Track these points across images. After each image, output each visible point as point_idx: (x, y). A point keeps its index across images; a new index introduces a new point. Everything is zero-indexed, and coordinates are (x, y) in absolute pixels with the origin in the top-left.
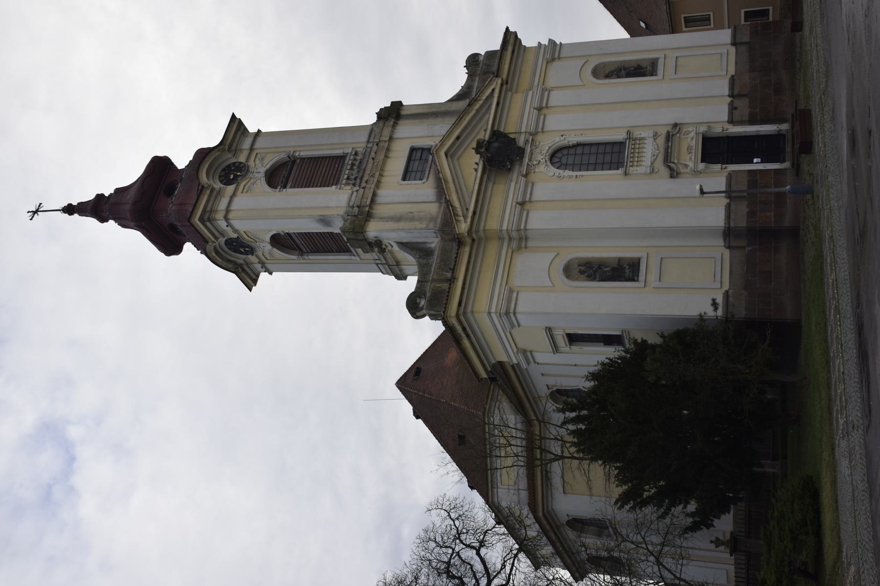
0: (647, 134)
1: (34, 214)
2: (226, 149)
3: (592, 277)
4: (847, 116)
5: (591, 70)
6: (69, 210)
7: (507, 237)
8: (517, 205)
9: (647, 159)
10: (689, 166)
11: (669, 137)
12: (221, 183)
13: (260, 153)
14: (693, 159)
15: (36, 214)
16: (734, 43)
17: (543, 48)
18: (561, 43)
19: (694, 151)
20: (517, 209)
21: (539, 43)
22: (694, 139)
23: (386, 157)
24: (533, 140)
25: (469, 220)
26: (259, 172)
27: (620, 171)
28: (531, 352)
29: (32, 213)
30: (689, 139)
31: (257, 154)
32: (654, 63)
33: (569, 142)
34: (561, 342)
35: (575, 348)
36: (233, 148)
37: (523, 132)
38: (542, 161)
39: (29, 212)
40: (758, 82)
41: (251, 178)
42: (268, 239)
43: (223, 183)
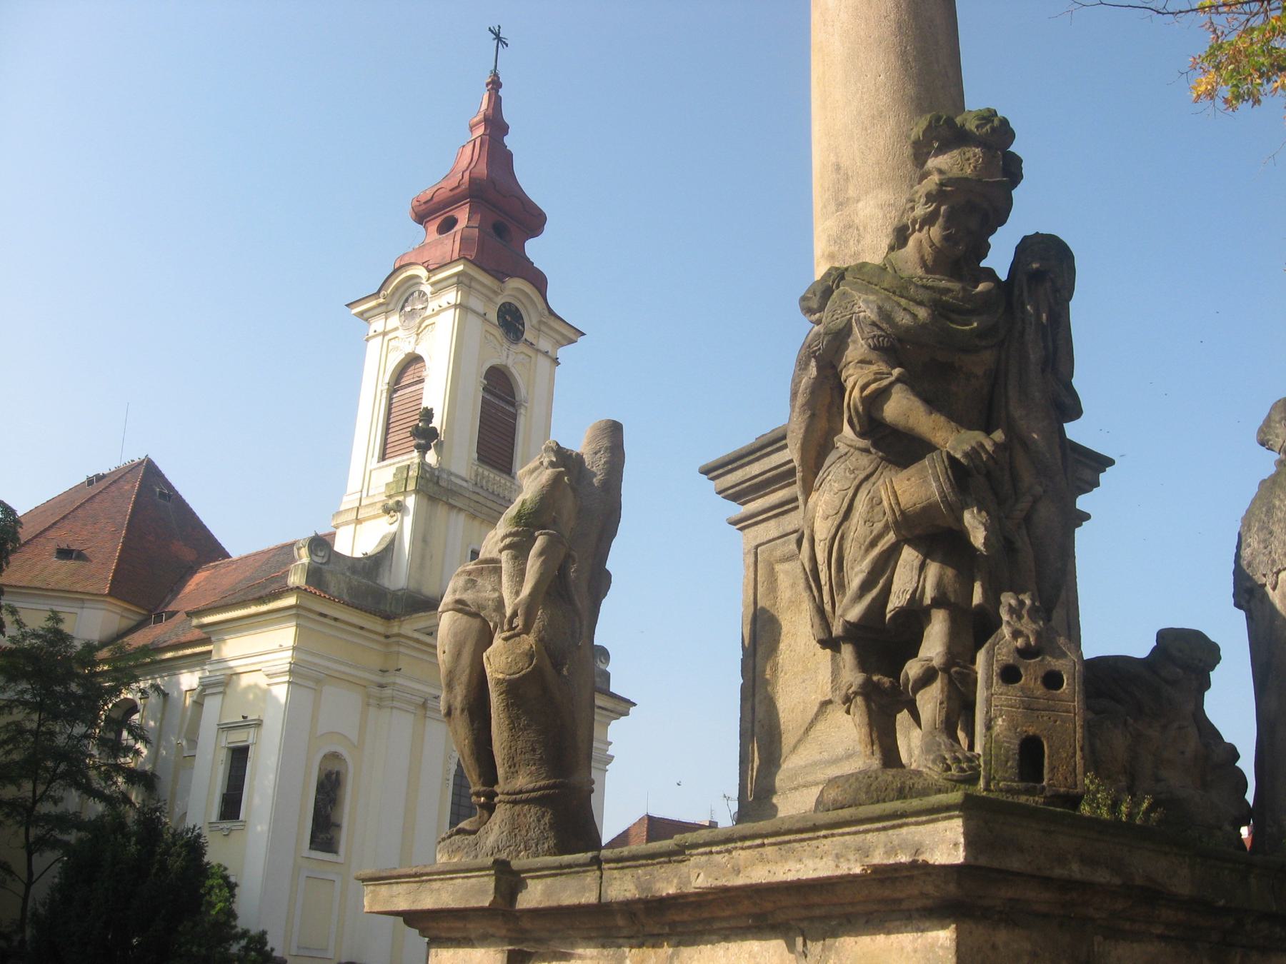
1: (495, 34)
2: (543, 319)
3: (321, 787)
4: (932, 814)
6: (495, 84)
8: (423, 700)
12: (502, 305)
13: (530, 362)
15: (494, 37)
21: (611, 743)
25: (416, 635)
26: (507, 357)
28: (224, 693)
29: (500, 44)
31: (530, 357)
34: (238, 738)
35: (223, 756)
36: (543, 328)
39: (499, 27)
41: (502, 346)
42: (418, 352)
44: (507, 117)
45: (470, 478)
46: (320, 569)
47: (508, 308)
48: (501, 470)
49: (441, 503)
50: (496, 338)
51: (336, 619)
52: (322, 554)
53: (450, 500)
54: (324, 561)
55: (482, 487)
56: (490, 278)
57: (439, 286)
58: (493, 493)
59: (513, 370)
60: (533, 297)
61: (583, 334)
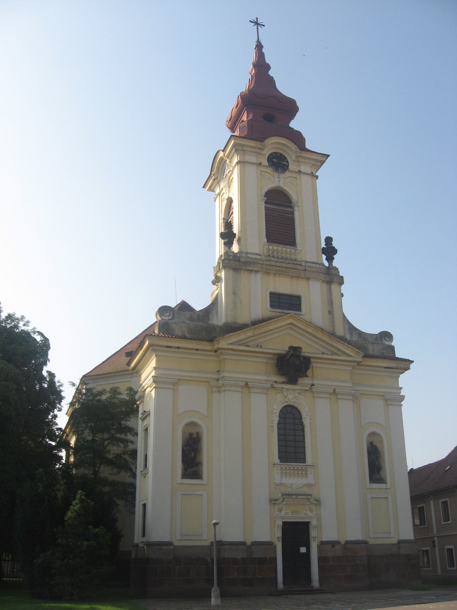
0: (310, 479)
5: (375, 431)
7: (219, 377)
8: (245, 383)
9: (289, 481)
10: (280, 513)
11: (308, 496)
14: (287, 515)
16: (400, 542)
17: (397, 391)
18: (402, 405)
19: (294, 515)
20: (241, 383)
21: (401, 388)
22: (305, 516)
23: (292, 277)
24: (306, 390)
25: (230, 347)
26: (279, 182)
27: (277, 461)
30: (306, 512)
32: (382, 480)
33: (305, 418)
36: (300, 159)
37: (313, 382)
38: (287, 398)
40: (358, 562)
43: (270, 156)
44: (268, 60)
45: (263, 253)
46: (167, 323)
47: (271, 157)
48: (290, 245)
49: (243, 270)
50: (269, 174)
51: (178, 348)
52: (168, 314)
53: (248, 268)
54: (170, 317)
55: (273, 256)
56: (253, 141)
57: (230, 157)
58: (282, 258)
59: (285, 188)
60: (287, 144)
61: (328, 156)
